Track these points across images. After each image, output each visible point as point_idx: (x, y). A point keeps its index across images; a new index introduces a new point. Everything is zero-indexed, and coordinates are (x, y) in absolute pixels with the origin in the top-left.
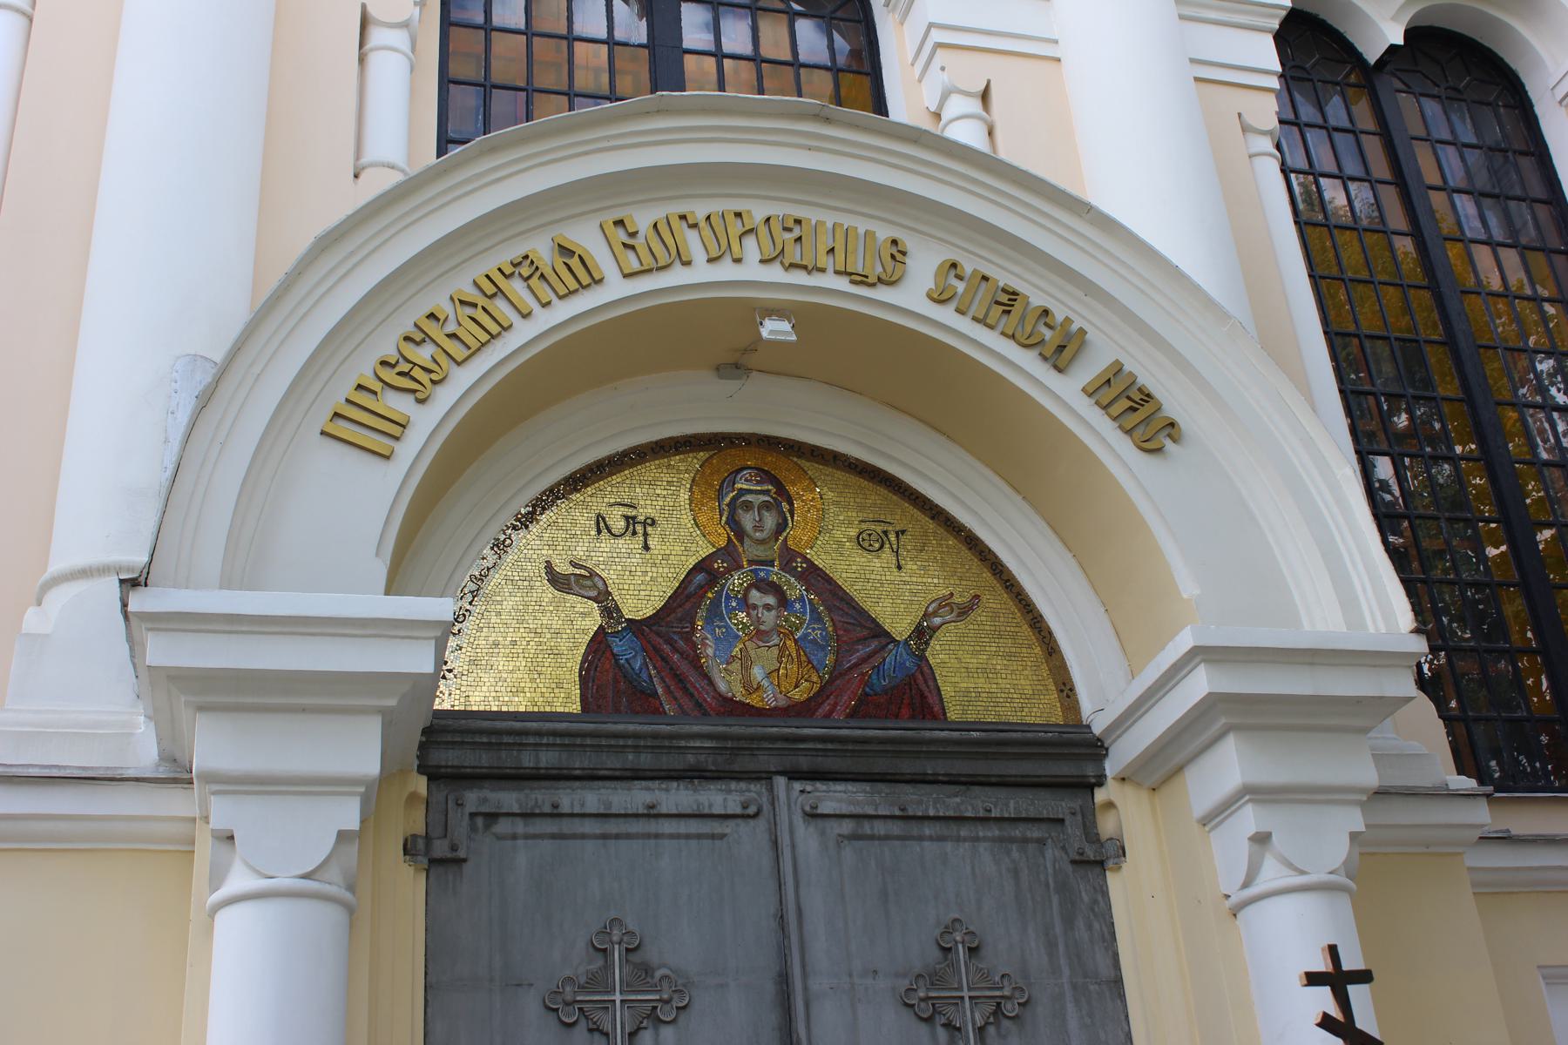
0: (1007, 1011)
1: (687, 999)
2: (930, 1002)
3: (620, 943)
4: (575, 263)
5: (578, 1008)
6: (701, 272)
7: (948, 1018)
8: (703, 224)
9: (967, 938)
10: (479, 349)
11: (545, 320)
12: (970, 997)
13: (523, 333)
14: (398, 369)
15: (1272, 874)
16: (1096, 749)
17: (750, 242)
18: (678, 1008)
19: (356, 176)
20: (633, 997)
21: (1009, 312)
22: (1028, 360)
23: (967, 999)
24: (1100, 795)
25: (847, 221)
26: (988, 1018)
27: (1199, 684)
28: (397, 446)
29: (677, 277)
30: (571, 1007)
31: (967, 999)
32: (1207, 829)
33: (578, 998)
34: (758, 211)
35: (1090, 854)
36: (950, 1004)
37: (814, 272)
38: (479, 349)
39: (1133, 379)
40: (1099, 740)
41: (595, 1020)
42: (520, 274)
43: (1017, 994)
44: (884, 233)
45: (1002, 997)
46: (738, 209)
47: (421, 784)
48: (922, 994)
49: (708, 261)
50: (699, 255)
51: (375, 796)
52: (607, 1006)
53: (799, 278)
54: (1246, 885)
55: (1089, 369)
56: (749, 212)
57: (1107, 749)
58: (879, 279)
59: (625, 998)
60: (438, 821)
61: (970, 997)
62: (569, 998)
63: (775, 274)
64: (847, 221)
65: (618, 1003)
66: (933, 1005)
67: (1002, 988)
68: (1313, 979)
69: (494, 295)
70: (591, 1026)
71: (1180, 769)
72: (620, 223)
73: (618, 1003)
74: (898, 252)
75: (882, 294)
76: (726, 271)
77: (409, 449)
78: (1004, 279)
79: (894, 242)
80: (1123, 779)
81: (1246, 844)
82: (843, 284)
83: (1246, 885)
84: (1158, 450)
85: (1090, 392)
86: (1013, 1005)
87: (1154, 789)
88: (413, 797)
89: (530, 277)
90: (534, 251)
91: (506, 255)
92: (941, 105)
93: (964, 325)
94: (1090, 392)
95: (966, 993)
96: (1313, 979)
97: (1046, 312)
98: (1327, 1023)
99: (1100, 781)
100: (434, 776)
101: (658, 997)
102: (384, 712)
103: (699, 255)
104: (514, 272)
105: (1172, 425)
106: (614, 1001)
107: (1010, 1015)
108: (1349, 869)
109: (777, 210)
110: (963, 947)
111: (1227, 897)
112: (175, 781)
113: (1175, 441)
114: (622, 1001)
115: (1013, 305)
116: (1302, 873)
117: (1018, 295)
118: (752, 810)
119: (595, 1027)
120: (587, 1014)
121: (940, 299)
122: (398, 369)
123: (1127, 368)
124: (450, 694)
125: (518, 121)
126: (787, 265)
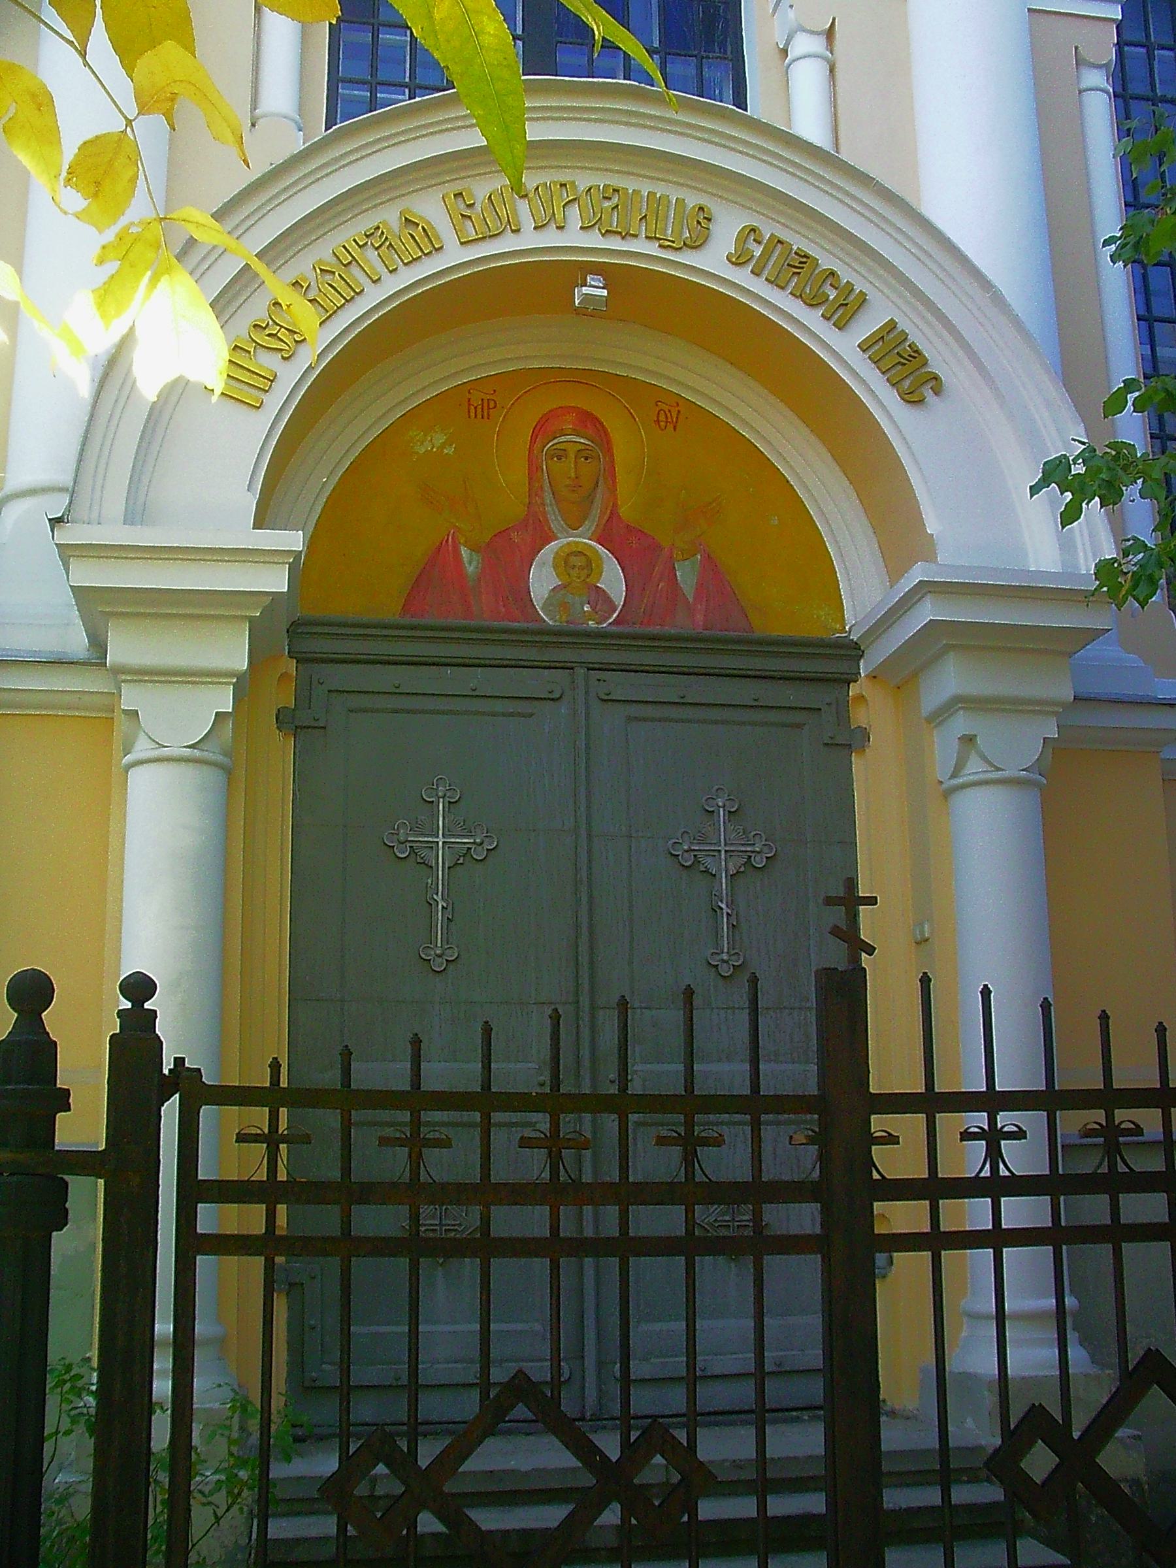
0: (755, 861)
1: (495, 843)
2: (692, 854)
3: (443, 797)
4: (418, 233)
5: (410, 847)
6: (530, 239)
7: (706, 867)
8: (531, 195)
9: (727, 803)
10: (335, 312)
11: (393, 285)
12: (726, 851)
13: (373, 296)
14: (267, 332)
15: (974, 768)
16: (853, 651)
17: (574, 211)
18: (487, 850)
19: (253, 125)
20: (453, 840)
21: (799, 273)
22: (812, 319)
23: (723, 852)
24: (854, 690)
25: (660, 190)
26: (740, 867)
27: (927, 612)
28: (265, 398)
29: (507, 244)
30: (404, 845)
31: (723, 852)
32: (932, 725)
33: (409, 839)
34: (584, 181)
35: (839, 740)
36: (709, 855)
37: (628, 238)
38: (335, 312)
39: (904, 336)
40: (856, 643)
41: (422, 856)
42: (372, 243)
43: (766, 849)
44: (693, 200)
45: (752, 852)
46: (563, 180)
47: (292, 666)
48: (686, 847)
49: (535, 228)
50: (528, 224)
51: (244, 686)
52: (432, 846)
53: (615, 244)
54: (953, 776)
55: (867, 326)
56: (573, 183)
57: (863, 652)
58: (684, 243)
59: (446, 840)
60: (304, 695)
61: (726, 851)
62: (402, 839)
63: (594, 240)
64: (660, 190)
65: (440, 843)
66: (695, 856)
67: (754, 844)
68: (829, 901)
69: (350, 263)
70: (419, 860)
71: (915, 675)
72: (458, 195)
73: (440, 843)
74: (704, 217)
75: (686, 258)
76: (551, 238)
77: (275, 400)
78: (798, 243)
79: (701, 209)
80: (875, 677)
81: (956, 743)
82: (652, 249)
83: (953, 776)
84: (920, 402)
85: (864, 347)
86: (762, 858)
87: (899, 688)
88: (284, 676)
89: (380, 246)
90: (385, 223)
91: (366, 223)
92: (787, 44)
93: (758, 286)
94: (864, 347)
95: (722, 848)
96: (829, 901)
97: (833, 274)
98: (836, 932)
99: (854, 677)
100: (302, 660)
101: (472, 841)
102: (251, 620)
103: (528, 224)
104: (367, 242)
105: (936, 378)
106: (438, 842)
107: (757, 866)
108: (1037, 767)
109: (600, 180)
110: (724, 810)
111: (941, 782)
112: (96, 664)
113: (937, 393)
114: (444, 842)
115: (803, 268)
116: (998, 769)
117: (808, 258)
118: (556, 695)
119: (422, 861)
120: (416, 851)
121: (738, 260)
122: (267, 332)
123: (900, 327)
124: (699, 222)
125: (378, 106)
126: (603, 232)
